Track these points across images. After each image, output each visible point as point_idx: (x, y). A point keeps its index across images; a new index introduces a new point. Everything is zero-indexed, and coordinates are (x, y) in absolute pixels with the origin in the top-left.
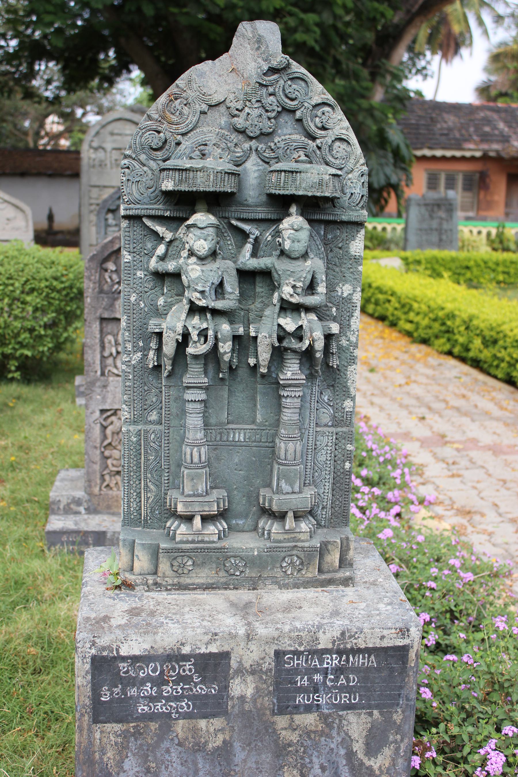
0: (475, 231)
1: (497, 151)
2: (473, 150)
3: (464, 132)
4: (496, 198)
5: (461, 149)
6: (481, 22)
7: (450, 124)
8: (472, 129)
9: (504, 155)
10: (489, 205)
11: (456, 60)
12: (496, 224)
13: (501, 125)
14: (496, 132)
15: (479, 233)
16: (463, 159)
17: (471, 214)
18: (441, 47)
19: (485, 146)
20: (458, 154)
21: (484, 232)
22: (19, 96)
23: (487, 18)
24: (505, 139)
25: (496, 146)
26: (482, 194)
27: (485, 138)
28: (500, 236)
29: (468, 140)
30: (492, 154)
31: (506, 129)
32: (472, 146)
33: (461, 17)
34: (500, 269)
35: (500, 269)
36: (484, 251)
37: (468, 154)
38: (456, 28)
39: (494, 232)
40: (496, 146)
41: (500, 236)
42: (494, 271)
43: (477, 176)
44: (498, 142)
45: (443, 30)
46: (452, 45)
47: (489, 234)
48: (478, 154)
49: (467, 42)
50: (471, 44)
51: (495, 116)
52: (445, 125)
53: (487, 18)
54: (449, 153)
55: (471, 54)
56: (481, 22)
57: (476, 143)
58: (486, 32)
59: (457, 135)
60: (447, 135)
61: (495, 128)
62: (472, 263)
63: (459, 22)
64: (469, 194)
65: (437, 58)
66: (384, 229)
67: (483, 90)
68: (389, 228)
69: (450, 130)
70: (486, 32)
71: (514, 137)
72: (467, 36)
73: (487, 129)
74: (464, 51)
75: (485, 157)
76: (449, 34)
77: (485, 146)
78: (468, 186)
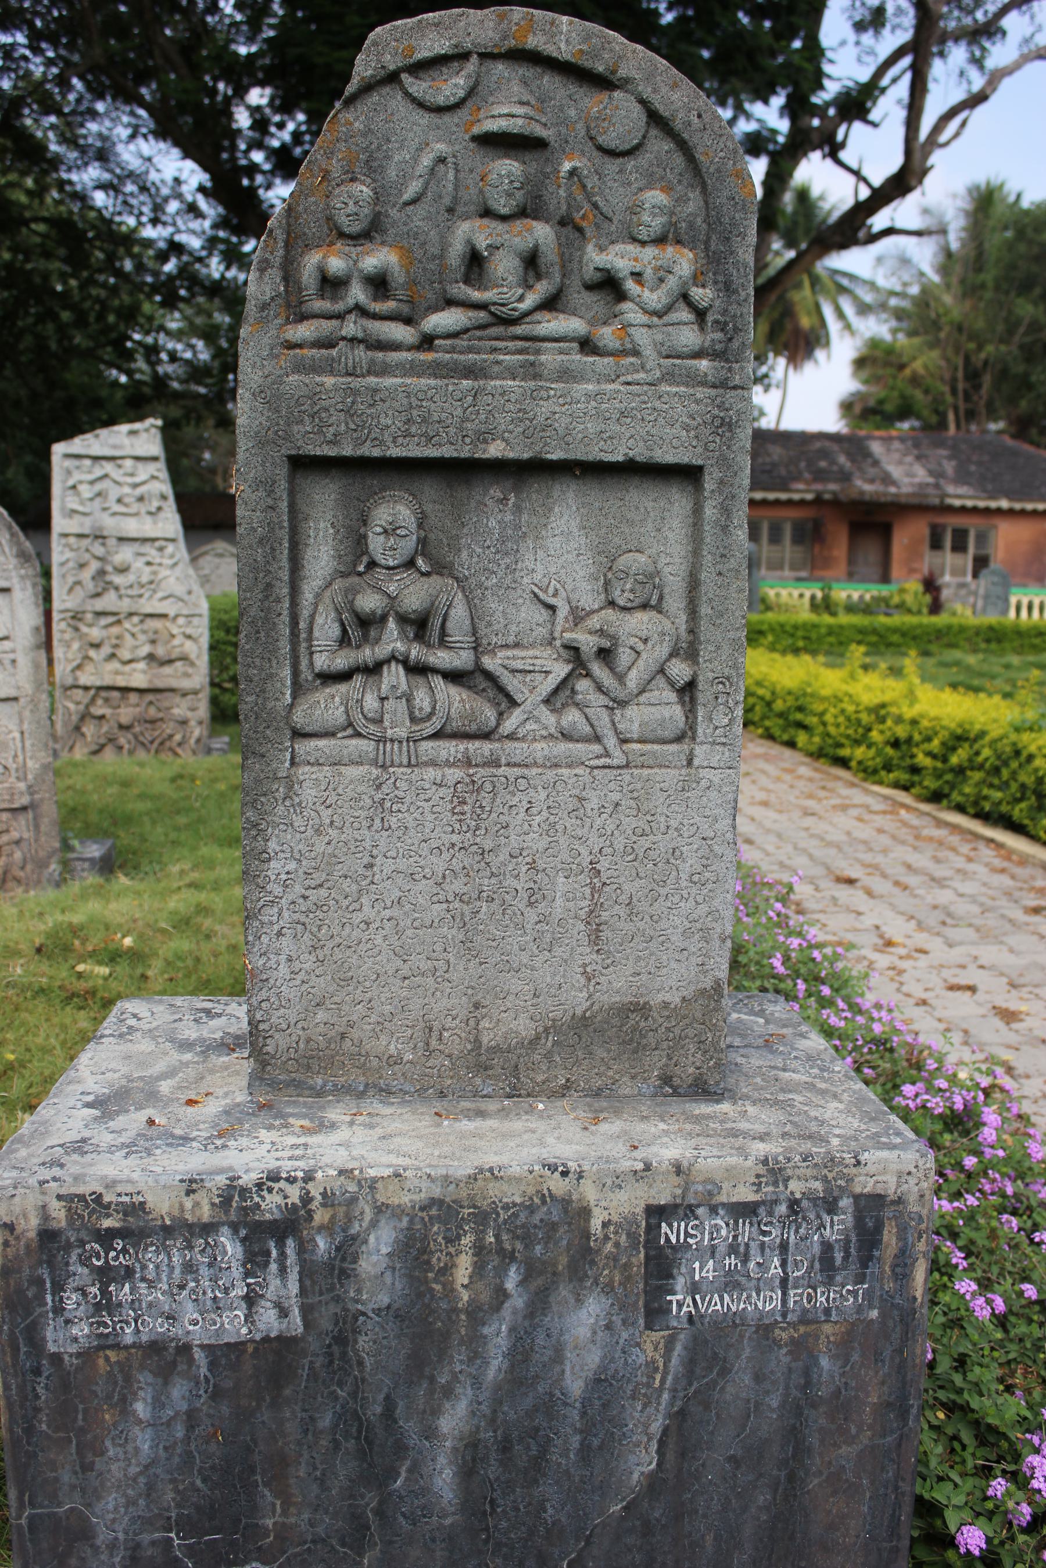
0: (796, 593)
1: (834, 493)
2: (802, 491)
3: (792, 468)
4: (835, 553)
5: (785, 489)
6: (840, 315)
7: (776, 458)
8: (803, 464)
9: (842, 497)
10: (827, 563)
11: (809, 367)
12: (820, 585)
13: (842, 459)
14: (835, 468)
15: (801, 596)
16: (790, 503)
17: (803, 574)
18: (786, 347)
19: (818, 487)
20: (783, 496)
21: (808, 594)
22: (211, 422)
23: (847, 306)
24: (845, 477)
25: (833, 487)
26: (817, 549)
27: (820, 476)
28: (826, 598)
29: (797, 478)
30: (827, 496)
31: (848, 464)
32: (801, 486)
33: (812, 306)
34: (800, 633)
35: (800, 633)
36: (805, 615)
37: (796, 497)
38: (805, 322)
39: (819, 595)
40: (833, 487)
41: (826, 598)
42: (792, 635)
43: (810, 526)
44: (836, 481)
45: (789, 326)
46: (802, 343)
47: (813, 598)
48: (809, 497)
49: (823, 341)
50: (827, 344)
51: (835, 447)
52: (768, 460)
53: (847, 306)
54: (771, 496)
55: (829, 357)
56: (840, 315)
57: (807, 483)
58: (848, 327)
59: (783, 472)
60: (769, 472)
61: (833, 462)
62: (765, 627)
63: (809, 314)
64: (799, 548)
65: (782, 362)
66: (778, 595)
67: (847, 407)
68: (784, 593)
69: (774, 465)
70: (848, 327)
71: (857, 474)
72: (822, 333)
73: (823, 464)
74: (820, 354)
75: (818, 501)
76: (797, 331)
77: (818, 487)
78: (798, 538)
